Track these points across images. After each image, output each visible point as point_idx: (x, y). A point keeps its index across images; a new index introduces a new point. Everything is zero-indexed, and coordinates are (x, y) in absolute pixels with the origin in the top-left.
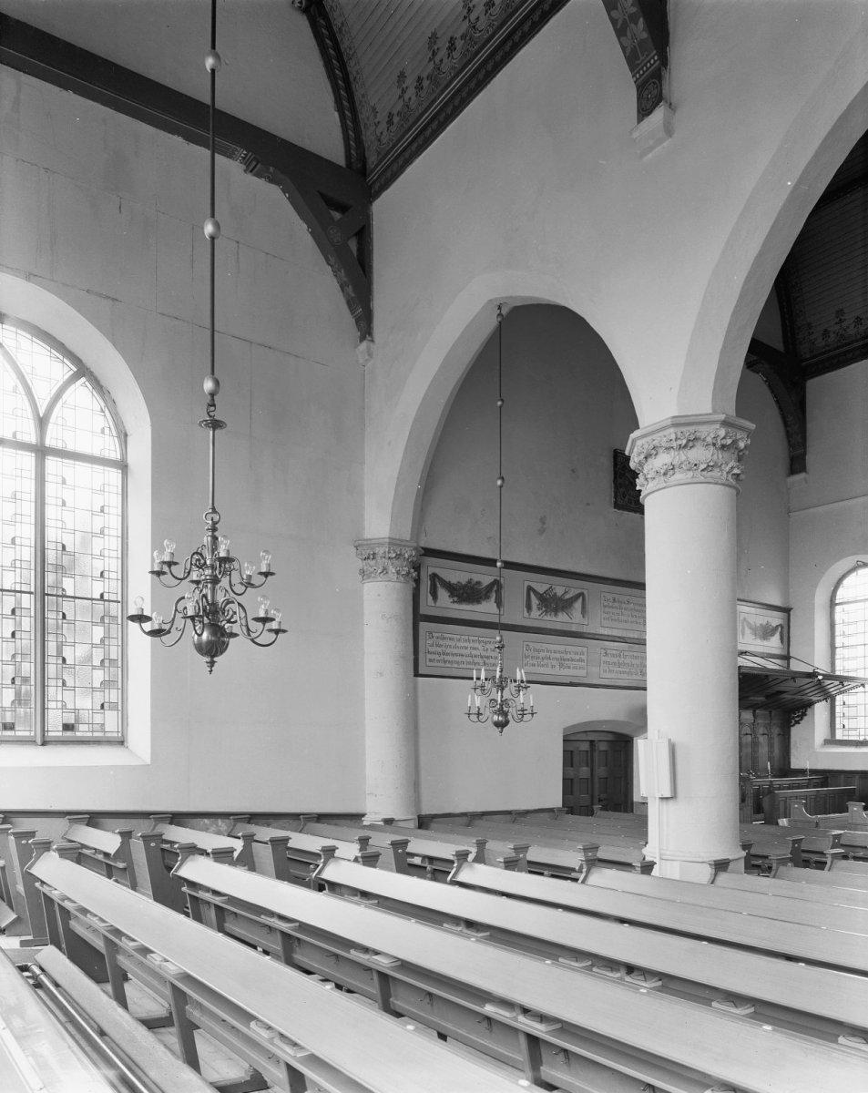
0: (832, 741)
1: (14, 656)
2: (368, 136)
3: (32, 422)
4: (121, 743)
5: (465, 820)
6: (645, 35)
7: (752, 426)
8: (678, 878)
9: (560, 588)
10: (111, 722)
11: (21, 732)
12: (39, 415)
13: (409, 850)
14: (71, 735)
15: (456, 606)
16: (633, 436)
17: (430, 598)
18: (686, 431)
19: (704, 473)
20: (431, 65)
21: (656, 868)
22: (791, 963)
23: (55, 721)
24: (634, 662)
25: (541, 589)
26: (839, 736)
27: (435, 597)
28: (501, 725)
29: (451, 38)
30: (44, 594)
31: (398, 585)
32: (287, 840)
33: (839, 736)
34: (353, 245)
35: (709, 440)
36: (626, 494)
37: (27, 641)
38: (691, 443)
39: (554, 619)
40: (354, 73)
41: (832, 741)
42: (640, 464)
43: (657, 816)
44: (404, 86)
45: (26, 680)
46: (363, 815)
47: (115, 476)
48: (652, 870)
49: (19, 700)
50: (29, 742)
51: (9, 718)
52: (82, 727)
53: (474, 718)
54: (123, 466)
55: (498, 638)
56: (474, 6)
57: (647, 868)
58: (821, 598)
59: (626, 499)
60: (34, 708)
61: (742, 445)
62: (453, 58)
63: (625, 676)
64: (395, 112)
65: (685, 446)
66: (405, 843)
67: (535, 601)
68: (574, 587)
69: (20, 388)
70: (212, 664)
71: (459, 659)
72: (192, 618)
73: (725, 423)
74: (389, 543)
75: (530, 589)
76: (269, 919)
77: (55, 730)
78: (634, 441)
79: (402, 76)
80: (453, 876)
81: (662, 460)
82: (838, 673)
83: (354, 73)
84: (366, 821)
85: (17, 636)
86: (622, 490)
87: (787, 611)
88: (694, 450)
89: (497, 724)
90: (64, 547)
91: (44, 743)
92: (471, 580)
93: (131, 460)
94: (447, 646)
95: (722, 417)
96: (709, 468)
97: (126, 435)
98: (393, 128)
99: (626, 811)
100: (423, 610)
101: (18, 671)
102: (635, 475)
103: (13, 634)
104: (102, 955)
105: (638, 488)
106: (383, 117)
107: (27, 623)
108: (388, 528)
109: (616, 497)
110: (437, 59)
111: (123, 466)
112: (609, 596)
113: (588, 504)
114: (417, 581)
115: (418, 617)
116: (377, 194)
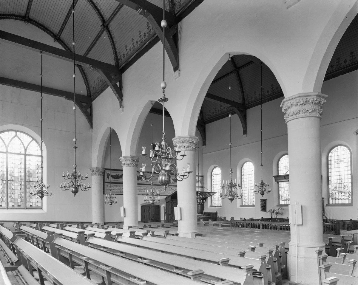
0: (212, 206)
1: (20, 193)
2: (91, 89)
3: (24, 150)
4: (41, 208)
5: (116, 223)
6: (118, 96)
7: (327, 96)
10: (40, 205)
11: (22, 207)
12: (90, 109)
14: (31, 207)
15: (113, 180)
16: (284, 100)
17: (107, 178)
18: (304, 99)
19: (310, 113)
20: (140, 38)
21: (179, 235)
22: (163, 253)
23: (10, 205)
26: (213, 205)
27: (108, 178)
30: (26, 181)
31: (99, 177)
33: (213, 205)
34: (118, 84)
35: (311, 101)
37: (23, 190)
38: (305, 103)
40: (176, 8)
41: (212, 206)
42: (286, 110)
45: (23, 197)
46: (92, 222)
48: (147, 235)
49: (21, 201)
54: (42, 156)
55: (152, 183)
57: (177, 235)
58: (209, 174)
60: (24, 202)
61: (322, 103)
65: (303, 104)
66: (134, 232)
69: (21, 144)
70: (75, 195)
73: (318, 96)
74: (131, 157)
77: (28, 206)
78: (284, 102)
81: (294, 109)
82: (213, 191)
83: (176, 8)
84: (93, 223)
85: (21, 189)
87: (202, 176)
88: (306, 105)
89: (110, 204)
90: (30, 172)
91: (26, 209)
92: (117, 174)
93: (43, 155)
95: (317, 93)
96: (188, 147)
99: (159, 222)
100: (105, 181)
101: (21, 195)
102: (284, 114)
103: (20, 189)
104: (69, 259)
105: (285, 118)
107: (23, 187)
108: (96, 166)
114: (104, 176)
115: (104, 182)
116: (93, 101)
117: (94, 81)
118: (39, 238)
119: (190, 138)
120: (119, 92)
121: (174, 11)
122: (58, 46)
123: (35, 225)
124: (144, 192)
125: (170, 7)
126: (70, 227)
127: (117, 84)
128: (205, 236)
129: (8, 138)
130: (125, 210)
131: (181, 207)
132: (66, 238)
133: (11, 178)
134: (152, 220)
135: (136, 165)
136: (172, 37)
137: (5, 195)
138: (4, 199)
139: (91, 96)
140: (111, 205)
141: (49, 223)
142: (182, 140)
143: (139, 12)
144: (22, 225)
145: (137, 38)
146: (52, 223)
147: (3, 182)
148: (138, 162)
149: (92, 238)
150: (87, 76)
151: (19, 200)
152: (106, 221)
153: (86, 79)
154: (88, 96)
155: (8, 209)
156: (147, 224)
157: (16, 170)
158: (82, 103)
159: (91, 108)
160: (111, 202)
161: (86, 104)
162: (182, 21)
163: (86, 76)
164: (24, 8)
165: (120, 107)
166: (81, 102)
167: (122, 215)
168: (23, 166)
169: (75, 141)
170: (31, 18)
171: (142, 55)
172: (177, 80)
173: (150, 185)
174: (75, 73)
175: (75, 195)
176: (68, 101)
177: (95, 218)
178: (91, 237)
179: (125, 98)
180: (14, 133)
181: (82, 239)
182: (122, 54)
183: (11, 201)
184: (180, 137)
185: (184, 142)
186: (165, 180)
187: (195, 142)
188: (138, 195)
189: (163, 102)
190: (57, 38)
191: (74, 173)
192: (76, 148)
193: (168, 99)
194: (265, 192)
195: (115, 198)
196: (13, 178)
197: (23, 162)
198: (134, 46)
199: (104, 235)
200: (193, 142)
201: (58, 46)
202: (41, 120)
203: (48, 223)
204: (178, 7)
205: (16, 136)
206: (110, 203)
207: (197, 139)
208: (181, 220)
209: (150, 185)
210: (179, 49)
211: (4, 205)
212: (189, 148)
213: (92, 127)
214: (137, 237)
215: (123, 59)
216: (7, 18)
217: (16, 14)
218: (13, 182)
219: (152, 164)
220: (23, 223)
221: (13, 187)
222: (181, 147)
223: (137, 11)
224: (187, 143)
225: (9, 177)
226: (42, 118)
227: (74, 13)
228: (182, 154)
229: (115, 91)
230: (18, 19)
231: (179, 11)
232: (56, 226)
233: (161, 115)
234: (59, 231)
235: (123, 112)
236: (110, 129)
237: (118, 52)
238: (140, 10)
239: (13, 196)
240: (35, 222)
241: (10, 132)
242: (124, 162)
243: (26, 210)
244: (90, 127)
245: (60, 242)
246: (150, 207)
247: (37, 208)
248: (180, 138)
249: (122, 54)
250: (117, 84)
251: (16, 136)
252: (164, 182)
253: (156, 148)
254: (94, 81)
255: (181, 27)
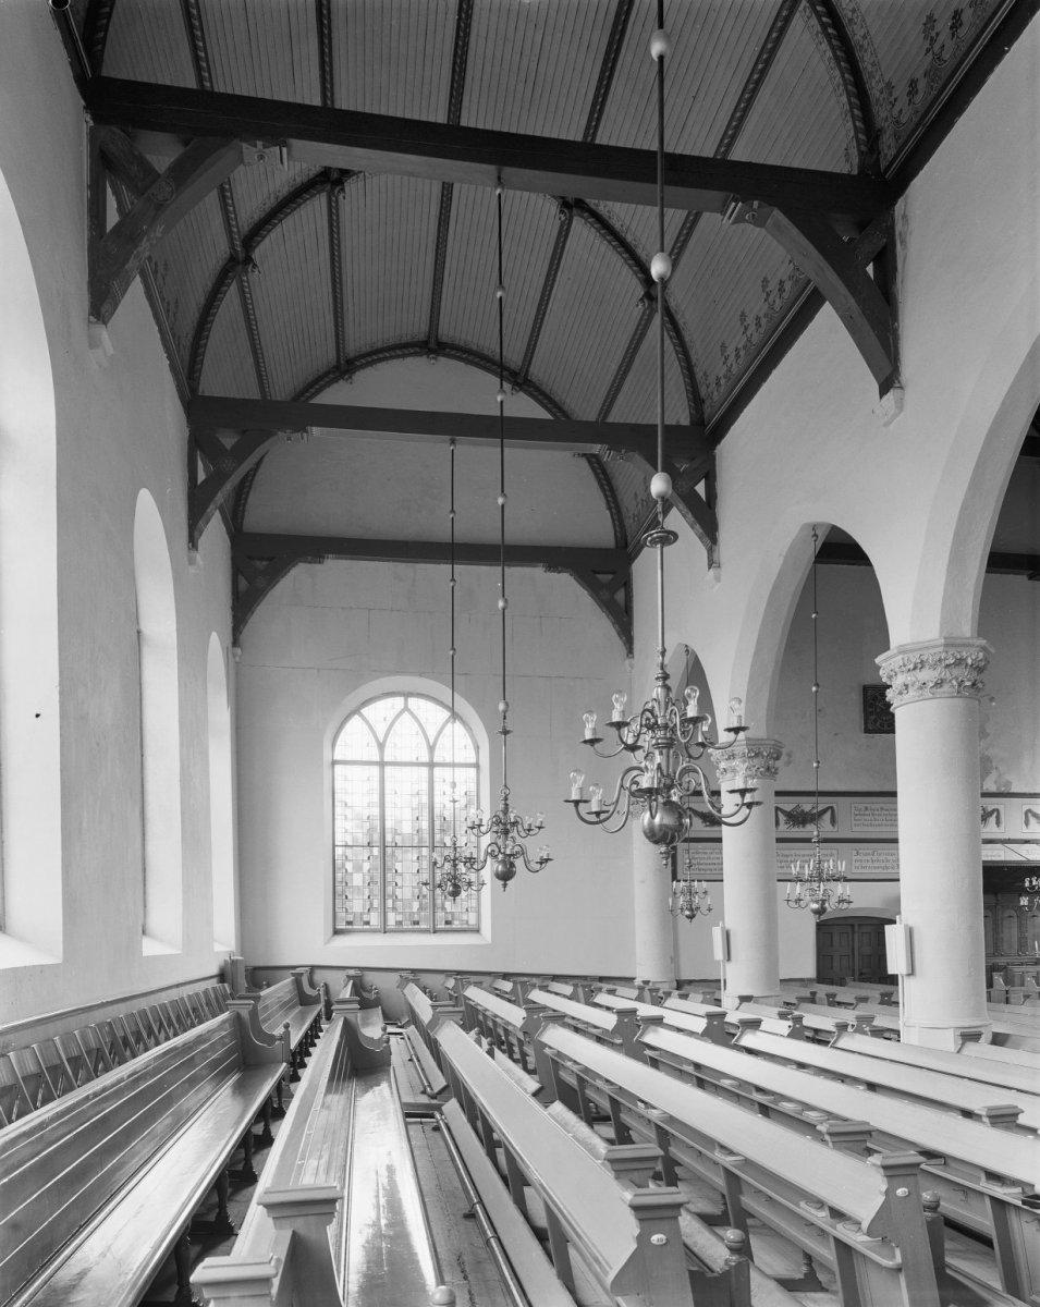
2: (628, 522)
4: (478, 931)
6: (701, 531)
8: (917, 1044)
9: (807, 805)
10: (472, 919)
13: (726, 1020)
15: (708, 829)
23: (392, 918)
24: (889, 858)
25: (788, 808)
28: (691, 917)
29: (956, 12)
30: (385, 847)
32: (634, 1011)
34: (701, 488)
36: (877, 714)
39: (802, 829)
43: (909, 991)
44: (768, 290)
45: (425, 896)
47: (473, 771)
49: (421, 908)
50: (426, 931)
51: (416, 918)
52: (456, 922)
53: (792, 904)
54: (477, 766)
55: (815, 833)
56: (937, 34)
59: (878, 724)
62: (958, 37)
63: (880, 870)
64: (761, 315)
67: (782, 818)
68: (823, 803)
70: (505, 886)
71: (711, 867)
72: (440, 886)
75: (777, 809)
76: (813, 1211)
79: (743, 316)
80: (737, 1041)
86: (873, 717)
93: (481, 763)
94: (701, 859)
96: (939, 684)
97: (478, 747)
98: (740, 361)
106: (901, 90)
109: (866, 723)
110: (749, 333)
111: (477, 766)
112: (862, 806)
113: (836, 734)
117: (636, 494)
118: (510, 1028)
119: (946, 645)
120: (706, 518)
121: (878, 160)
122: (524, 407)
123: (507, 986)
124: (785, 870)
125: (861, 153)
126: (683, 1002)
127: (697, 488)
128: (1017, 1046)
129: (385, 719)
130: (727, 936)
131: (910, 924)
132: (579, 1028)
133: (394, 838)
134: (861, 974)
135: (768, 769)
136: (870, 269)
137: (377, 889)
138: (376, 903)
139: (626, 546)
140: (691, 917)
141: (546, 979)
142: (915, 658)
143: (731, 216)
144: (534, 986)
145: (757, 307)
146: (556, 978)
147: (372, 852)
148: (777, 758)
149: (656, 1031)
150: (613, 482)
151: (416, 905)
152: (685, 976)
153: (612, 490)
154: (617, 547)
155: (385, 932)
156: (844, 994)
157: (407, 815)
158: (598, 576)
159: (627, 585)
160: (691, 910)
161: (610, 577)
162: (907, 192)
163: (609, 483)
164: (423, 317)
165: (710, 567)
166: (595, 572)
167: (719, 954)
168: (425, 799)
169: (505, 712)
170: (444, 339)
171: (960, 111)
172: (891, 427)
173: (808, 840)
174: (503, 492)
175: (505, 886)
176: (554, 576)
177: (646, 967)
178: (653, 1027)
179: (724, 534)
180: (399, 702)
181: (628, 1036)
182: (712, 379)
183: (394, 909)
184: (903, 651)
185: (921, 665)
186: (661, 825)
187: (970, 661)
188: (779, 880)
189: (659, 546)
190: (519, 379)
191: (501, 816)
192: (506, 732)
193: (676, 536)
194: (519, 863)
195: (705, 893)
196: (398, 839)
197: (425, 786)
198: (749, 340)
199: (700, 1025)
200: (959, 662)
201: (524, 407)
202: (451, 652)
203: (547, 980)
204: (892, 142)
205: (406, 708)
206: (687, 913)
207: (984, 649)
208: (912, 973)
209: (808, 840)
210: (900, 298)
211: (375, 919)
212: (946, 687)
213: (630, 651)
214: (818, 1038)
215: (716, 396)
216: (380, 360)
217: (404, 340)
218: (398, 852)
219: (815, 765)
220: (473, 979)
221: (398, 866)
222: (910, 690)
223: (725, 215)
224: (934, 667)
225: (389, 838)
226: (453, 649)
227: (501, 298)
228: (731, 726)
229: (690, 515)
230: (410, 355)
231: (896, 157)
232: (568, 989)
233: (868, 567)
234: (646, 1010)
235: (719, 584)
236: (687, 650)
237: (699, 376)
238: (736, 207)
239: (398, 892)
240: (506, 976)
241: (390, 701)
242: (723, 765)
243: (433, 936)
244: (626, 651)
245: (557, 1038)
246: (853, 926)
247: (464, 931)
248: (904, 652)
249: (712, 379)
250: (697, 488)
251: (406, 708)
252: (661, 834)
253: (689, 708)
254: (636, 494)
255: (904, 217)
